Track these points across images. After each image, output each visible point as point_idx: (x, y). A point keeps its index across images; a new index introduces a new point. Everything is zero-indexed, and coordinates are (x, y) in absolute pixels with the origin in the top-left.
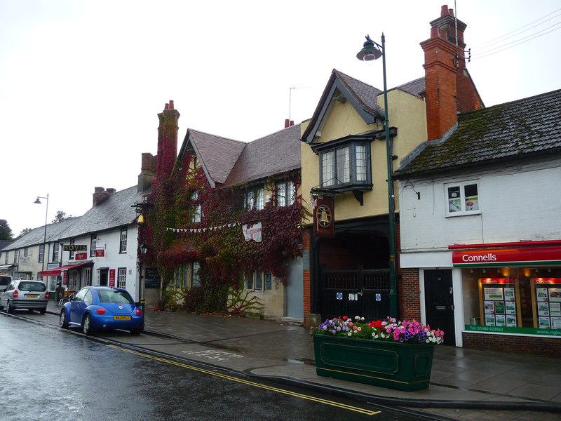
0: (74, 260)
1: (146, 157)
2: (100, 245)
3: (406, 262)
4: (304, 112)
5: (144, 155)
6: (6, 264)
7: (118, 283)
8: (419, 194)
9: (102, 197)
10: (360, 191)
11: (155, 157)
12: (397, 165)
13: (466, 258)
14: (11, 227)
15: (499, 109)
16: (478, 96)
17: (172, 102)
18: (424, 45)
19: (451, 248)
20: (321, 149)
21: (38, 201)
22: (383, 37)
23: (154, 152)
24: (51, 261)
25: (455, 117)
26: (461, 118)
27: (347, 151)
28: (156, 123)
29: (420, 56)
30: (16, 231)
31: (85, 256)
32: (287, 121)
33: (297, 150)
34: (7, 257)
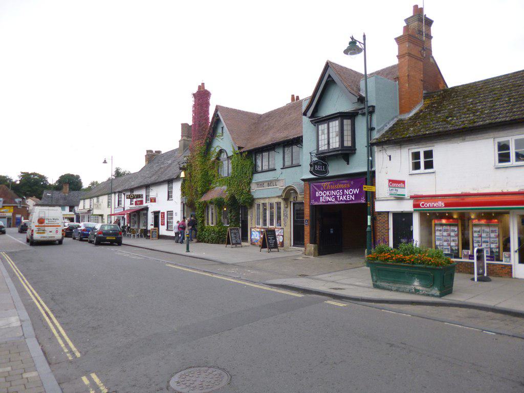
0: (134, 206)
1: (185, 126)
2: (153, 193)
3: (379, 207)
4: (306, 91)
5: (183, 125)
6: (84, 208)
7: (167, 222)
8: (390, 156)
9: (152, 157)
10: (346, 154)
11: (191, 126)
12: (376, 135)
13: (423, 205)
15: (454, 89)
16: (443, 79)
17: (203, 84)
18: (398, 40)
20: (317, 120)
21: (105, 162)
22: (364, 36)
24: (117, 206)
28: (191, 102)
29: (394, 49)
30: (85, 184)
31: (141, 202)
32: (293, 96)
33: (300, 123)
34: (84, 204)
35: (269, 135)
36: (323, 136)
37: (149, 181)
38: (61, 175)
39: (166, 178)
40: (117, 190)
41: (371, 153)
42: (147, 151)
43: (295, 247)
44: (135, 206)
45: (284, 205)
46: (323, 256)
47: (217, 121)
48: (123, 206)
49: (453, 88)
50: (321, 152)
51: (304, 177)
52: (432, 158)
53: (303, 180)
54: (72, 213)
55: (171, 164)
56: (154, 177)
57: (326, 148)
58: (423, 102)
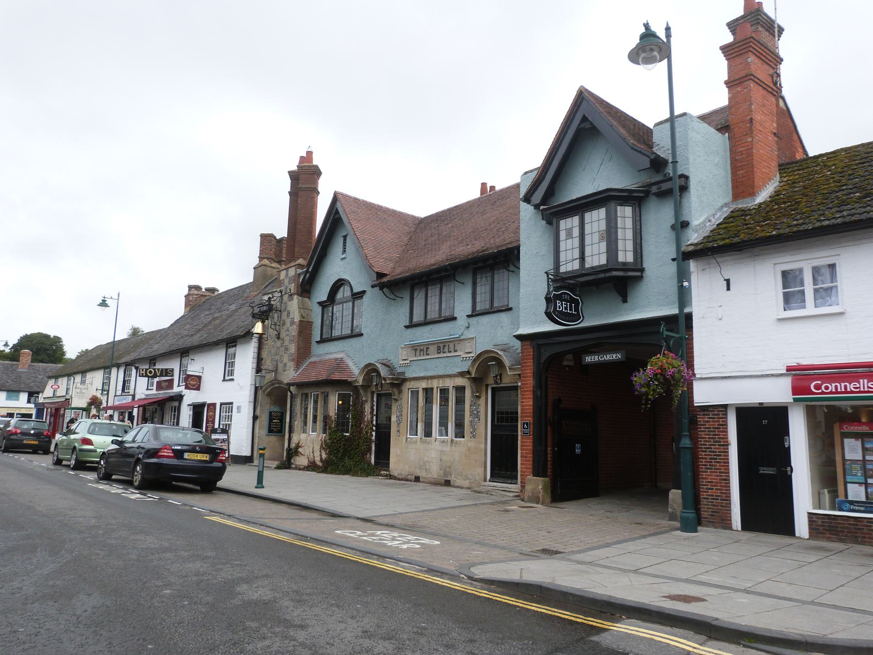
1: (266, 239)
2: (194, 367)
8: (728, 281)
11: (282, 239)
12: (693, 237)
14: (65, 348)
17: (309, 154)
19: (789, 369)
21: (104, 304)
22: (668, 29)
23: (281, 231)
24: (119, 393)
25: (774, 165)
26: (782, 168)
27: (602, 213)
30: (71, 351)
31: (170, 385)
35: (441, 252)
36: (569, 241)
37: (188, 342)
38: (22, 334)
39: (224, 335)
40: (123, 360)
41: (683, 275)
42: (191, 287)
43: (495, 484)
44: (156, 392)
45: (473, 393)
46: (560, 505)
47: (334, 219)
48: (132, 392)
49: (816, 157)
50: (430, 320)
51: (524, 330)
52: (804, 286)
53: (520, 337)
54: (32, 406)
55: (236, 310)
56: (198, 335)
57: (576, 265)
58: (778, 179)
